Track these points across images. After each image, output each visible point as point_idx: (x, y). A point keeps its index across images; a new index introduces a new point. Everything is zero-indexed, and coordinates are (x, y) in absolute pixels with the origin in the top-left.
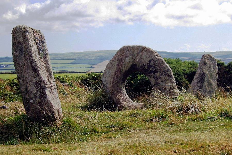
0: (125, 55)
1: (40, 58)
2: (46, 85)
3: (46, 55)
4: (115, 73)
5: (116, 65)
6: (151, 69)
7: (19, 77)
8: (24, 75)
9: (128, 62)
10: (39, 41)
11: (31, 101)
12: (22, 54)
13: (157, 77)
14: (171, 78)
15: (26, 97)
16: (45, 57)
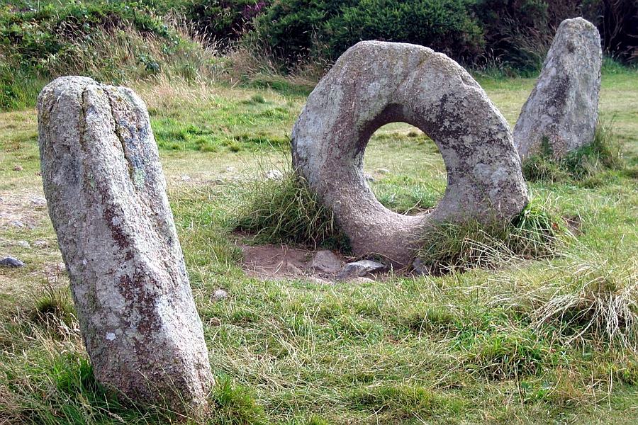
0: (365, 73)
1: (137, 188)
2: (158, 287)
3: (153, 177)
4: (335, 128)
5: (337, 100)
6: (447, 124)
7: (67, 256)
8: (86, 252)
9: (374, 96)
10: (131, 130)
11: (111, 337)
12: (76, 182)
13: (466, 148)
14: (508, 152)
15: (92, 323)
16: (151, 183)
